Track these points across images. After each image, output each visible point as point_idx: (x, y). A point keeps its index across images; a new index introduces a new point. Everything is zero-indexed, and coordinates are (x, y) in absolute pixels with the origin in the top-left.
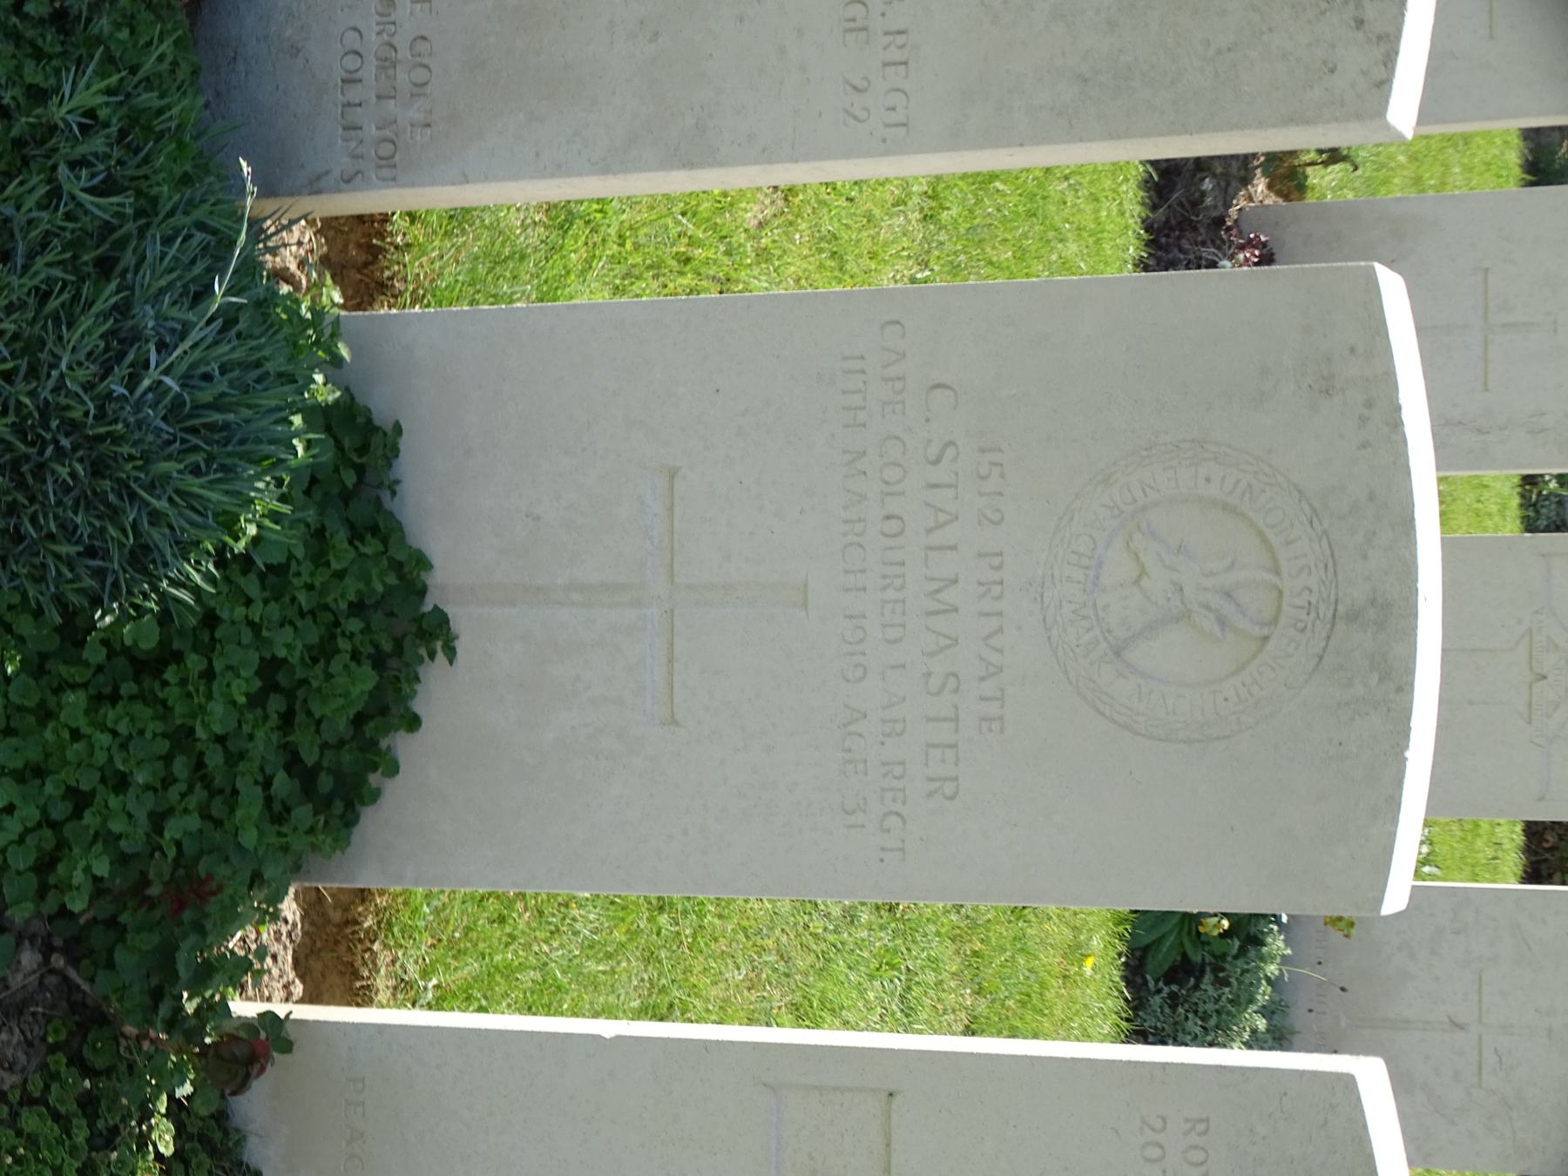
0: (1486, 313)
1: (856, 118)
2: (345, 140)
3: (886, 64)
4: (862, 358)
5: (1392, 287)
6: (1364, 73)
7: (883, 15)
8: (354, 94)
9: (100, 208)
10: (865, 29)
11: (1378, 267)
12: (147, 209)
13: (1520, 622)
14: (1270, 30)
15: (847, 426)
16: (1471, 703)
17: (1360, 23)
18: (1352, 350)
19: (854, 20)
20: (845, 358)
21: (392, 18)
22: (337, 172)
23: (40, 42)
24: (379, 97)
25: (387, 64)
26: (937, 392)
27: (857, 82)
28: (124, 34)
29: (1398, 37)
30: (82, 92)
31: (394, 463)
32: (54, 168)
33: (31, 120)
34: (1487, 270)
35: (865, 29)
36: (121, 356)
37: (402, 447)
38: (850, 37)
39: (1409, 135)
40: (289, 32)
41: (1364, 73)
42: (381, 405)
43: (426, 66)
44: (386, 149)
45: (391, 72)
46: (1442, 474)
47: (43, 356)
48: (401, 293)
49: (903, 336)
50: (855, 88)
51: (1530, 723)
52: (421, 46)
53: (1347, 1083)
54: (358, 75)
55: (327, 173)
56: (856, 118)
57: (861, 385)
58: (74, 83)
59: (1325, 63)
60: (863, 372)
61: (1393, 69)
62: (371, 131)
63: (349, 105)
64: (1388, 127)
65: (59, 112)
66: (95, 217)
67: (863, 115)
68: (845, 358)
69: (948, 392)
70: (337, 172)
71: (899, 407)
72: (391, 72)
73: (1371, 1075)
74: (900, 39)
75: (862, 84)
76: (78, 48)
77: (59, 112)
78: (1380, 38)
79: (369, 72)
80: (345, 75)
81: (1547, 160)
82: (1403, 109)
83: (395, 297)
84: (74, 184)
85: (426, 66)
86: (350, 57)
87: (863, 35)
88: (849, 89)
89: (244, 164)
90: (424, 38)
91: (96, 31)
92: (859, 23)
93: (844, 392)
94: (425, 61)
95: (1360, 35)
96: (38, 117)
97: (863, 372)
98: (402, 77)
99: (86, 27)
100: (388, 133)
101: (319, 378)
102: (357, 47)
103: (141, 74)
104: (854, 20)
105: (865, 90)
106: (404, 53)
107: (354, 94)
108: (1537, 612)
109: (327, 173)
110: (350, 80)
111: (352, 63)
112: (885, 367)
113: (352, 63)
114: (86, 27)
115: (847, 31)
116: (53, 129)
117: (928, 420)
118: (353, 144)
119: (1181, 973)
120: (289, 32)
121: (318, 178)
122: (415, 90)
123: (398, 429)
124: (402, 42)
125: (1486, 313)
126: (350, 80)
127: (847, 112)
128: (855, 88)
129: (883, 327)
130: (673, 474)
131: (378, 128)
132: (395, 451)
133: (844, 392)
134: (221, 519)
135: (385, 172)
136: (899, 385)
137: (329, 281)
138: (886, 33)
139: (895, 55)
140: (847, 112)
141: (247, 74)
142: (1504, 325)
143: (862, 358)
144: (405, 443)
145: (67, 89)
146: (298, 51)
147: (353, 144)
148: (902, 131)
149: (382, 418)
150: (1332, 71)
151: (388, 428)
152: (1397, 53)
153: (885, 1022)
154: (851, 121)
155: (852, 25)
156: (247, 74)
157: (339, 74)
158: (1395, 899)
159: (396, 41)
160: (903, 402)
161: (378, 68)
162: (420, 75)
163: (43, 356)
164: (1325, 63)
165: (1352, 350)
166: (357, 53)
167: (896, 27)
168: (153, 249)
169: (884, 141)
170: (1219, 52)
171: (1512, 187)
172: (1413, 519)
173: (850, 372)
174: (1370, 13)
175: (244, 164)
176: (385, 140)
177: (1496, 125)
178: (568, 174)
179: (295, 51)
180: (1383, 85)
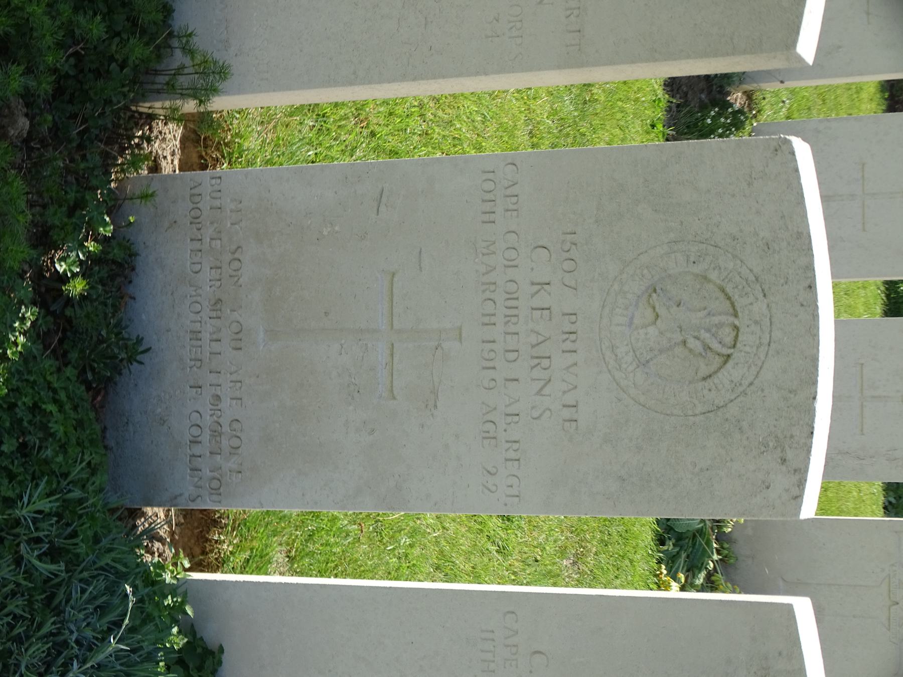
0: (862, 389)
1: (489, 490)
2: (191, 476)
3: (507, 460)
4: (493, 632)
6: (787, 490)
7: (505, 430)
8: (197, 450)
9: (45, 568)
10: (495, 438)
12: (73, 563)
13: (883, 570)
14: (731, 460)
15: (483, 671)
16: (854, 617)
17: (784, 461)
18: (780, 654)
19: (488, 432)
20: (482, 631)
21: (219, 407)
22: (186, 495)
23: (11, 467)
24: (211, 453)
25: (216, 434)
26: (537, 655)
27: (490, 469)
28: (60, 459)
29: (806, 471)
30: (37, 501)
31: (220, 669)
32: (18, 545)
33: (5, 517)
34: (862, 364)
35: (495, 438)
36: (59, 653)
37: (224, 660)
38: (486, 442)
39: (811, 63)
40: (159, 410)
41: (787, 490)
42: (211, 635)
43: (238, 437)
44: (215, 484)
45: (218, 439)
46: (837, 280)
47: (11, 661)
48: (226, 525)
49: (516, 622)
50: (488, 472)
51: (889, 630)
52: (236, 425)
53: (789, 608)
54: (199, 439)
55: (181, 495)
56: (489, 490)
57: (492, 648)
58: (30, 496)
59: (763, 482)
60: (493, 640)
61: (804, 489)
62: (206, 473)
63: (194, 456)
65: (23, 512)
66: (41, 573)
67: (494, 489)
68: (482, 631)
69: (543, 656)
70: (186, 495)
71: (514, 663)
72: (218, 439)
73: (803, 608)
74: (516, 446)
75: (494, 470)
76: (33, 466)
77: (23, 512)
78: (795, 471)
79: (206, 437)
80: (192, 438)
81: (902, 96)
82: (807, 46)
83: (222, 528)
84: (31, 556)
85: (238, 437)
86: (194, 428)
87: (493, 441)
88: (485, 472)
89: (127, 587)
90: (237, 420)
91: (44, 456)
92: (491, 435)
93: (482, 651)
94: (238, 434)
95: (784, 468)
96: (10, 515)
97: (493, 640)
99: (38, 452)
100: (216, 474)
101: (175, 630)
102: (198, 422)
103: (70, 479)
104: (488, 432)
105: (495, 474)
106: (226, 429)
107: (197, 450)
108: (893, 565)
109: (181, 495)
110: (195, 442)
111: (195, 431)
112: (506, 638)
113: (195, 431)
114: (38, 452)
115: (484, 438)
116: (17, 522)
117: (531, 672)
118: (196, 479)
119: (701, 107)
120: (159, 410)
121: (176, 498)
122: (233, 451)
123: (221, 650)
125: (862, 389)
127: (484, 486)
128: (488, 472)
129: (505, 614)
131: (210, 471)
132: (220, 663)
133: (482, 651)
135: (214, 497)
136: (514, 650)
137: (182, 555)
138: (507, 442)
139: (512, 455)
140: (484, 486)
141: (134, 433)
142: (873, 397)
143: (493, 632)
144: (225, 658)
145: (26, 499)
146: (164, 422)
147: (196, 479)
148: (516, 499)
149: (212, 644)
150: (768, 488)
151: (216, 650)
152: (806, 480)
154: (486, 491)
155: (487, 435)
156: (134, 433)
157: (188, 438)
159: (221, 420)
160: (516, 660)
161: (210, 435)
162: (235, 442)
163: (11, 661)
164: (763, 482)
165: (780, 654)
166: (199, 426)
167: (514, 439)
168: (76, 586)
169: (506, 505)
170: (701, 470)
171: (878, 317)
172: (825, 219)
173: (486, 639)
174: (790, 455)
175: (127, 587)
176: (214, 478)
177: (871, 280)
179: (163, 422)
180: (798, 498)
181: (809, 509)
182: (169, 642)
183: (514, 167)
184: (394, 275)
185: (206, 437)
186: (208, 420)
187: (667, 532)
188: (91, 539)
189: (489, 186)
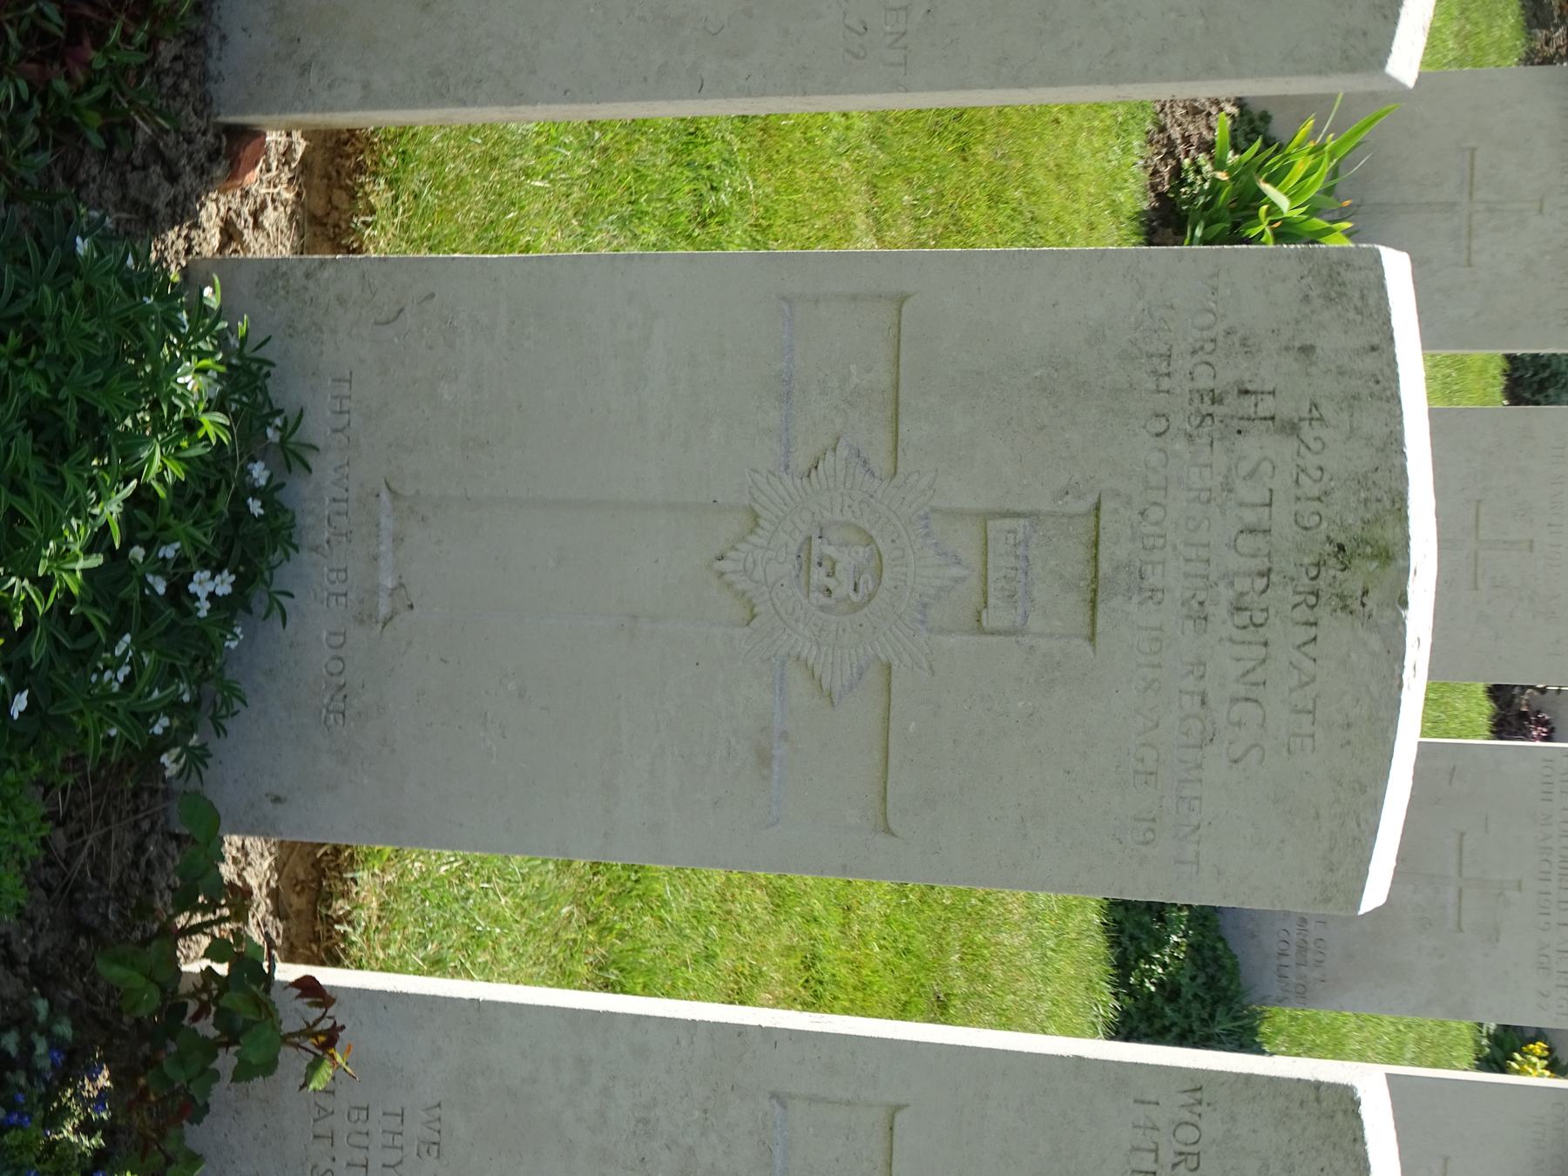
5: (1397, 267)
8: (1285, 961)
11: (1383, 250)
25: (1303, 948)
44: (1300, 989)
53: (1345, 1101)
62: (1293, 980)
64: (1390, 79)
79: (1293, 951)
98: (1310, 955)
106: (1311, 945)
107: (1285, 961)
110: (1282, 954)
111: (1283, 946)
124: (1311, 940)
126: (1282, 954)
130: (1446, 1159)
134: (56, 482)
153: (789, 1002)
158: (1375, 894)
162: (1320, 957)
177: (1478, 355)
178: (573, 101)
181: (1375, 894)
182: (151, 1016)
183: (1162, 455)
184: (1462, 835)
185: (1293, 951)
186: (1295, 937)
187: (1132, 927)
188: (128, 837)
189: (1547, 771)
